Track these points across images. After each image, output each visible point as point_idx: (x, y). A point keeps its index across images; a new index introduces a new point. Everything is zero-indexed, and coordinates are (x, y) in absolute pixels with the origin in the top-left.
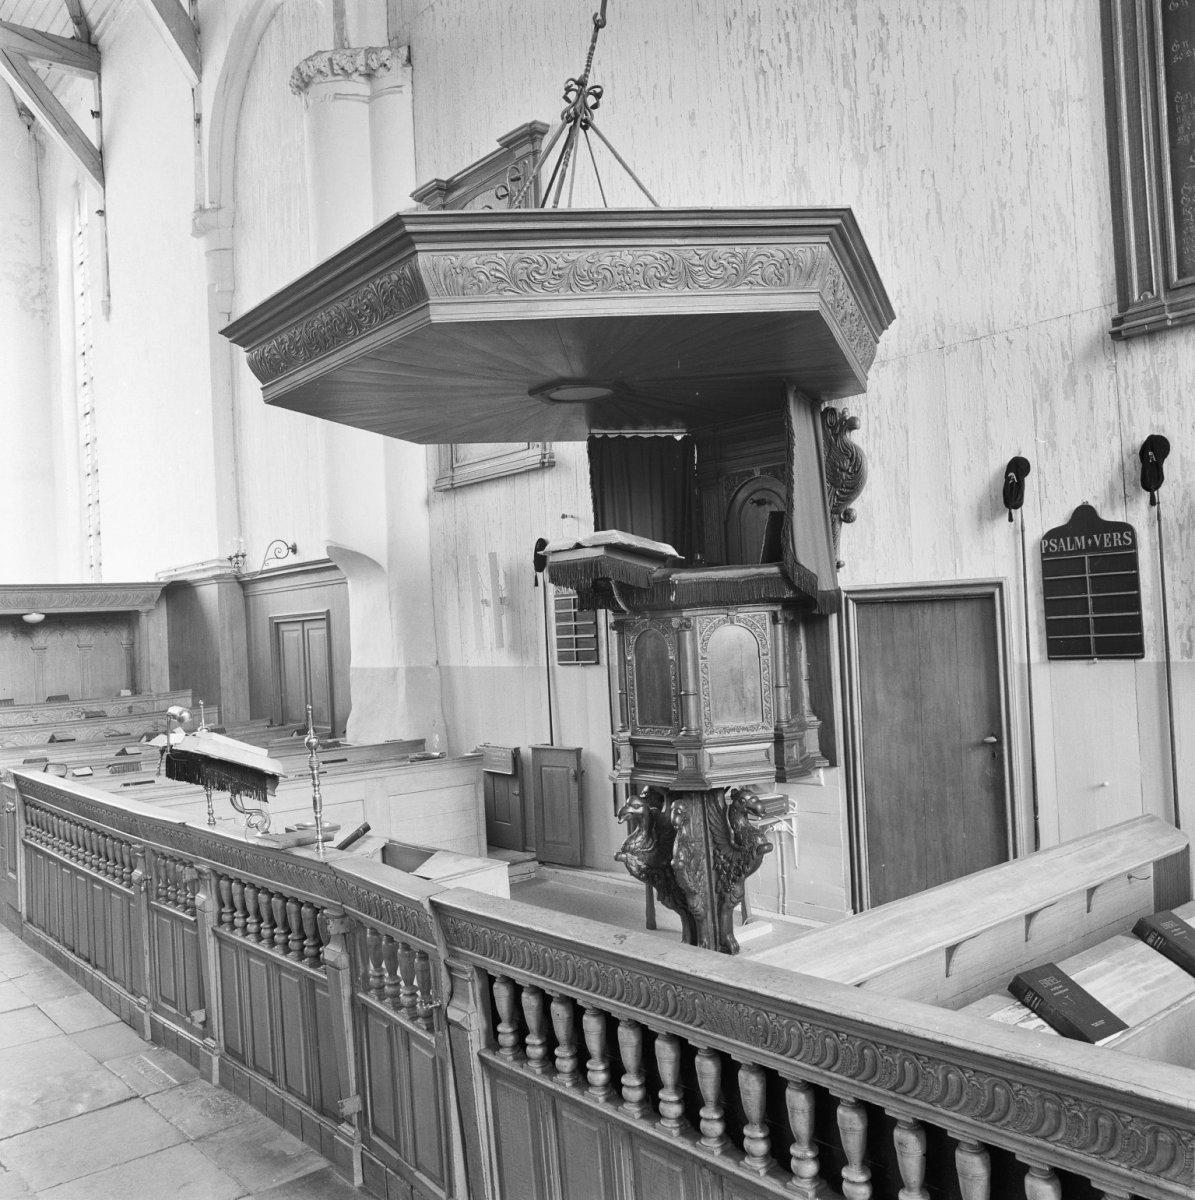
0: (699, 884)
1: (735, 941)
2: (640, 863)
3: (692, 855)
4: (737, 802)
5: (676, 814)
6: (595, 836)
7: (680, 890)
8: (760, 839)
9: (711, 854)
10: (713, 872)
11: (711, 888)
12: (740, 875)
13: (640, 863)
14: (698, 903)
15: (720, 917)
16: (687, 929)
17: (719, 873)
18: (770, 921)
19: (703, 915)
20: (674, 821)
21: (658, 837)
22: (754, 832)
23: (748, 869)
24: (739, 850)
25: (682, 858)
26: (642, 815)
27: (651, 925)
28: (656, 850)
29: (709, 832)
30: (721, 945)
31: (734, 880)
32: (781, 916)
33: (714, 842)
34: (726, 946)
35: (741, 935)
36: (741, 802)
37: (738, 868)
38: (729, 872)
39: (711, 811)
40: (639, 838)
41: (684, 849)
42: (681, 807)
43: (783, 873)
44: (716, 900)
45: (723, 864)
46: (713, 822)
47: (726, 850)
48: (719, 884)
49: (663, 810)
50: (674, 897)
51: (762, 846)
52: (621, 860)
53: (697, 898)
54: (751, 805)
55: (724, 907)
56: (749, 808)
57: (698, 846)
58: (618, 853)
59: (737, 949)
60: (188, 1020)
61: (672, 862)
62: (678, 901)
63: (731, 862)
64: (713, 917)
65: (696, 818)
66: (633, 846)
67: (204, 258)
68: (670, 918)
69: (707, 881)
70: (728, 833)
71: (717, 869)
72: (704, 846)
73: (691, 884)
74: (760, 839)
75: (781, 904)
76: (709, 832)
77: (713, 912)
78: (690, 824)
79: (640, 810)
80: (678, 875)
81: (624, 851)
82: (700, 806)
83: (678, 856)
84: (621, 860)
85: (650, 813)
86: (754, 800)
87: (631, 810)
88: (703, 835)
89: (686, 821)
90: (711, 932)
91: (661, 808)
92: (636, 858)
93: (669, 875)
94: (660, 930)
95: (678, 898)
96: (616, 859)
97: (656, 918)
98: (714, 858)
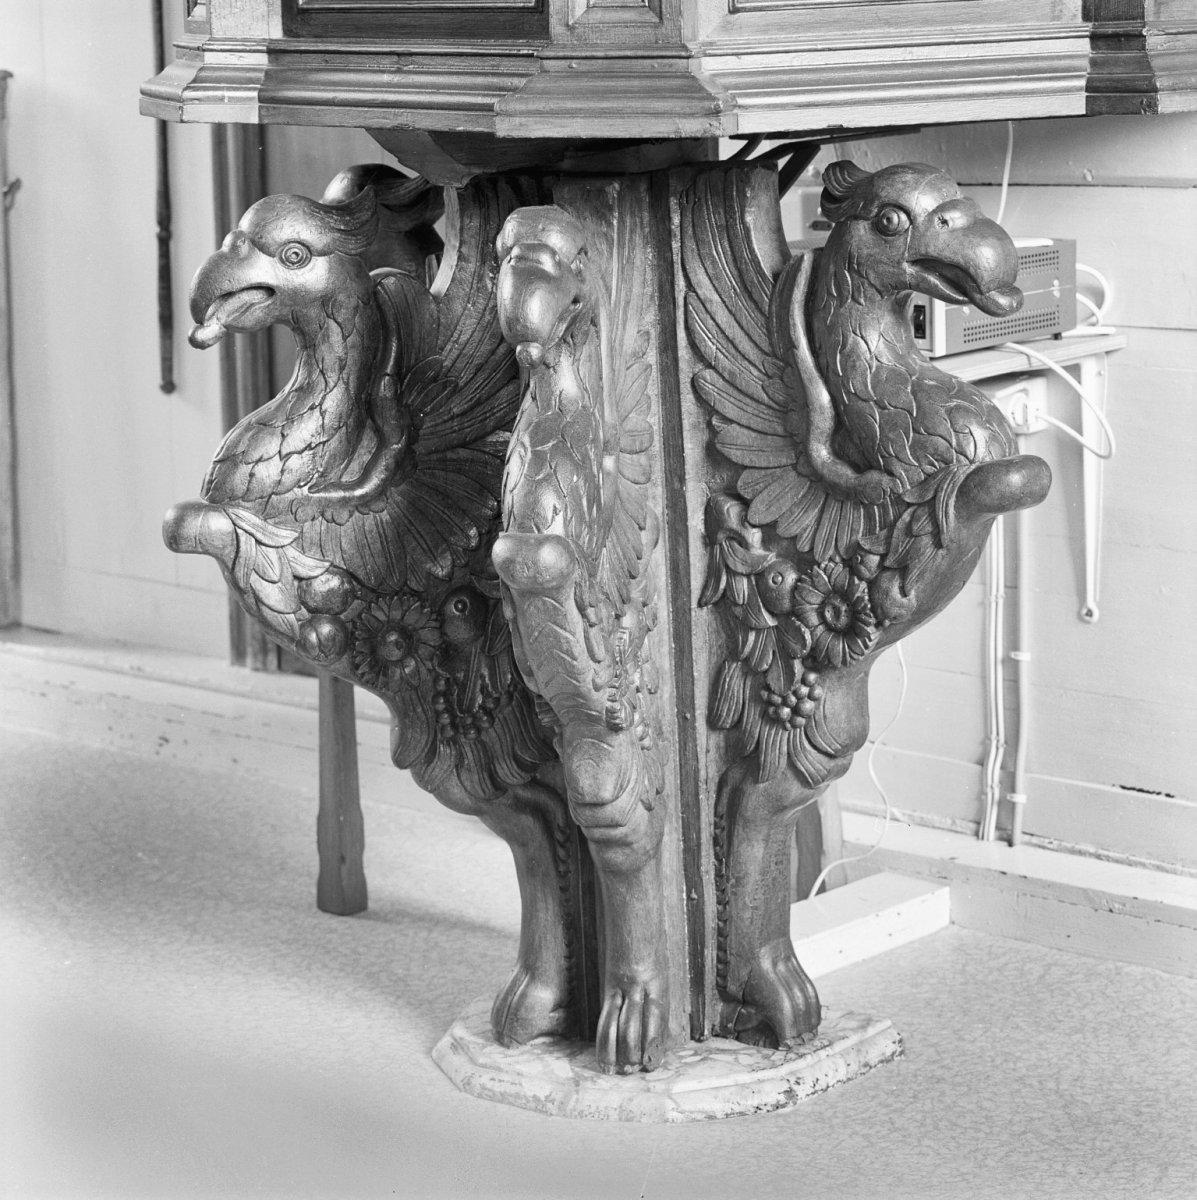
0: (623, 655)
1: (799, 976)
2: (308, 565)
3: (600, 515)
4: (861, 230)
5: (529, 276)
6: (556, 1055)
7: (527, 701)
8: (980, 434)
9: (696, 522)
10: (702, 620)
11: (684, 701)
12: (852, 632)
13: (308, 565)
14: (626, 782)
15: (725, 845)
16: (549, 917)
17: (731, 619)
18: (943, 873)
19: (643, 843)
20: (515, 320)
21: (412, 435)
22: (941, 402)
23: (899, 599)
24: (850, 496)
25: (557, 528)
26: (326, 301)
27: (343, 892)
28: (395, 495)
29: (688, 401)
30: (723, 993)
31: (818, 661)
32: (990, 852)
33: (713, 454)
34: (753, 1011)
35: (831, 943)
36: (882, 229)
37: (846, 594)
38: (790, 617)
39: (706, 289)
40: (307, 429)
41: (568, 477)
42: (556, 239)
43: (1013, 641)
44: (709, 767)
45: (759, 577)
46: (710, 347)
47: (777, 498)
48: (737, 684)
49: (441, 282)
50: (482, 746)
51: (981, 474)
52: (202, 547)
53: (620, 745)
54: (940, 243)
55: (755, 798)
56: (927, 263)
57: (634, 477)
58: (187, 510)
59: (810, 1017)
60: (141, 674)
61: (500, 548)
62: (507, 771)
63: (805, 563)
64: (691, 854)
65: (627, 324)
66: (268, 472)
67: (510, 1052)
68: (455, 864)
69: (666, 663)
70: (792, 407)
71: (723, 605)
72: (658, 475)
73: (592, 674)
74: (980, 434)
75: (994, 792)
76: (688, 401)
77: (690, 829)
78: (590, 327)
79: (316, 275)
80: (528, 621)
81: (218, 495)
82: (643, 257)
83: (531, 515)
84: (202, 547)
85: (372, 298)
86: (957, 219)
87: (264, 269)
88: (655, 419)
89: (577, 325)
90: (676, 930)
91: (424, 277)
92: (286, 535)
93: (460, 632)
94: (378, 917)
95: (499, 734)
96: (174, 540)
97: (368, 856)
98: (709, 540)
